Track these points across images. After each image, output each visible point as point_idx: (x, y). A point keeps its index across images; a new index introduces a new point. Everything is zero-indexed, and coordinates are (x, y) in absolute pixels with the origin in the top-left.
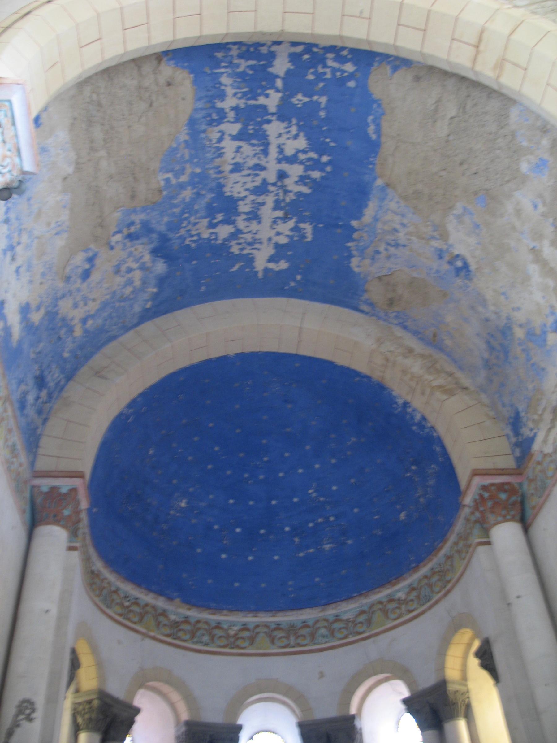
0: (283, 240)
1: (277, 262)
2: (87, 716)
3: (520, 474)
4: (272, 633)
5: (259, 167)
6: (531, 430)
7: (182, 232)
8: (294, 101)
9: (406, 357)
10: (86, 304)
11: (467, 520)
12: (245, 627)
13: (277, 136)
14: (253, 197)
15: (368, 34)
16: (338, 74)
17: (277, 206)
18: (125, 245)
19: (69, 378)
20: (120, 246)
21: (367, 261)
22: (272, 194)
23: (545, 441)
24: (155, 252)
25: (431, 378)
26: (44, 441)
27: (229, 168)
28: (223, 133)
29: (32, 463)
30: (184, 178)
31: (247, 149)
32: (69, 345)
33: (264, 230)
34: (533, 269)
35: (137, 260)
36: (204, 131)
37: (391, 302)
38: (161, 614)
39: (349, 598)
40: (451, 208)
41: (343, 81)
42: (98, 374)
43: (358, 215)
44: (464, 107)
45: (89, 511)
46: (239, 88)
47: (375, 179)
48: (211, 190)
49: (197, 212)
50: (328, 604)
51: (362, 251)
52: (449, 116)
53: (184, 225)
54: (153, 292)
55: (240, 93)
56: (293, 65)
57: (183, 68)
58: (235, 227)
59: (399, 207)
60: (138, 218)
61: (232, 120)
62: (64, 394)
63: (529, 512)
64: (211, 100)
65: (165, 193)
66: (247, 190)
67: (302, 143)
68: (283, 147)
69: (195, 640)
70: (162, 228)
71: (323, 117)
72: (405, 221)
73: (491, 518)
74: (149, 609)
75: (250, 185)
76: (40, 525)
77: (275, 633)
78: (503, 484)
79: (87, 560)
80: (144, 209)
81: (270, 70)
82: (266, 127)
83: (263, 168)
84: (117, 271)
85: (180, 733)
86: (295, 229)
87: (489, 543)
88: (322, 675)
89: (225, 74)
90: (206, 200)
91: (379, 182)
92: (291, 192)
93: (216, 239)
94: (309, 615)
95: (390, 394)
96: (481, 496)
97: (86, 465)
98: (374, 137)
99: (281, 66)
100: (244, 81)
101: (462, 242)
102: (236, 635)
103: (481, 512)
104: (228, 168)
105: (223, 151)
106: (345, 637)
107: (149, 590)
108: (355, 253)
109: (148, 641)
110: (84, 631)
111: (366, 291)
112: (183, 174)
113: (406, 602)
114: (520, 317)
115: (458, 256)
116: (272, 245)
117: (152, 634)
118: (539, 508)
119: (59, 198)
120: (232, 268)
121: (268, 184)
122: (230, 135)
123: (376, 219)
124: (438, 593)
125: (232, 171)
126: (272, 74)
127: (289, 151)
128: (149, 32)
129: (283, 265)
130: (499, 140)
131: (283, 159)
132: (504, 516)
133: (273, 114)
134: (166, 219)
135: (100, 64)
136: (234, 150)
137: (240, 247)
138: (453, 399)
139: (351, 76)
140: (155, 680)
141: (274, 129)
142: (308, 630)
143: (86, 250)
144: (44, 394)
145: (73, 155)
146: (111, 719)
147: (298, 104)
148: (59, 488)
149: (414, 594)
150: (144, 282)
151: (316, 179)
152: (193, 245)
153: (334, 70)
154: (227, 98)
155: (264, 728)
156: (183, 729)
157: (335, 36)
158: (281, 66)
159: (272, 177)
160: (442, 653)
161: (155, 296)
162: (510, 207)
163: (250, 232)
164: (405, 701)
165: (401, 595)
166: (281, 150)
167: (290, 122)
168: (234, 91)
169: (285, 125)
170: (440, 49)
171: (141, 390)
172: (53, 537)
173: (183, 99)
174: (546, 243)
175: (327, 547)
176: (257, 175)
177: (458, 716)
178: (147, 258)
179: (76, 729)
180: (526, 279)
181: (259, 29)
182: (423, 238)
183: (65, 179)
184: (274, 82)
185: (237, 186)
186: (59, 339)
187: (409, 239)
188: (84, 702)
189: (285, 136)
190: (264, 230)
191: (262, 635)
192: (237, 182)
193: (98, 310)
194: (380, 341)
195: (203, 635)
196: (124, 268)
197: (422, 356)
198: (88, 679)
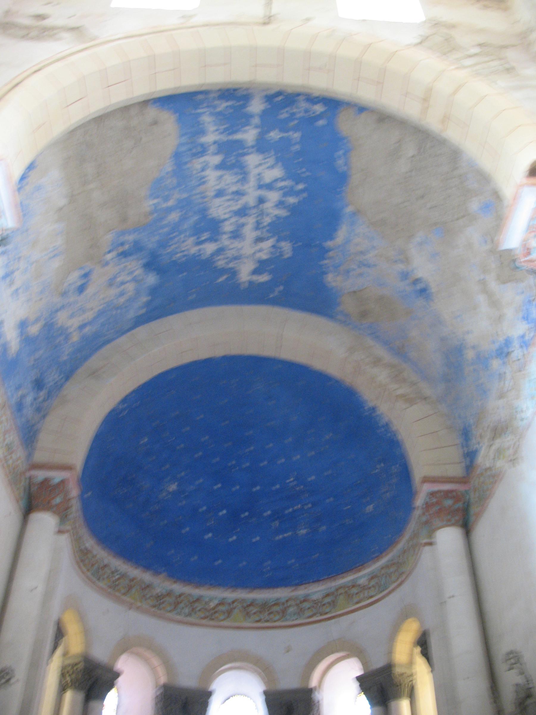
0: (264, 256)
3: (465, 483)
4: (247, 607)
5: (239, 194)
17: (258, 226)
19: (68, 377)
27: (212, 194)
29: (30, 455)
34: (481, 298)
37: (364, 314)
43: (331, 237)
45: (81, 497)
60: (131, 238)
77: (251, 608)
78: (451, 491)
79: (77, 540)
85: (158, 693)
87: (431, 544)
88: (288, 650)
91: (349, 209)
94: (281, 593)
99: (256, 107)
101: (423, 268)
102: (214, 608)
105: (206, 179)
110: (71, 603)
118: (478, 515)
129: (264, 278)
141: (252, 160)
144: (42, 394)
146: (92, 681)
150: (138, 293)
156: (161, 691)
158: (256, 107)
161: (148, 304)
165: (362, 581)
168: (215, 128)
170: (391, 101)
172: (45, 522)
175: (303, 532)
178: (139, 272)
179: (62, 689)
185: (219, 209)
198: (75, 644)
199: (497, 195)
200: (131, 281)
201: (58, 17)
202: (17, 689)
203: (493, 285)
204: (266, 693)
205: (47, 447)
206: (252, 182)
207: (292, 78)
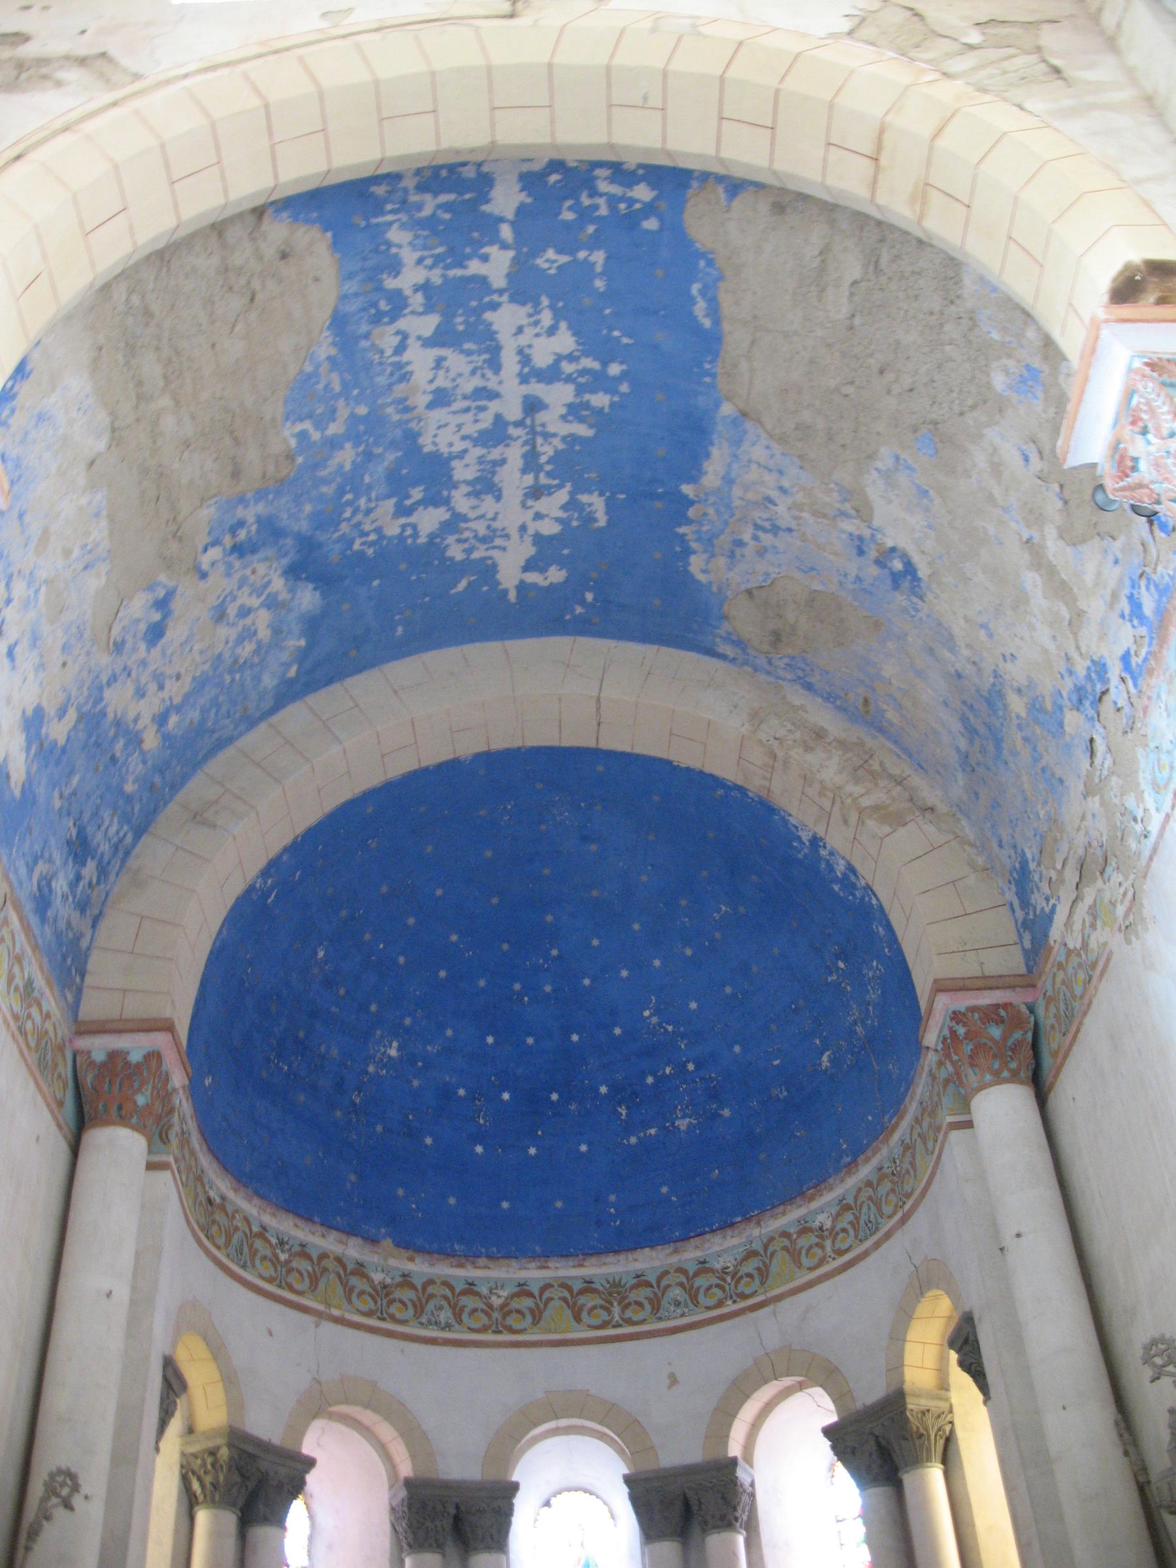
0: (549, 528)
1: (543, 570)
2: (208, 1479)
4: (575, 1299)
5: (486, 394)
6: (1047, 899)
7: (344, 527)
8: (540, 262)
9: (808, 748)
10: (161, 687)
12: (523, 1290)
13: (514, 331)
14: (479, 451)
15: (664, 140)
16: (622, 206)
17: (531, 462)
18: (230, 566)
20: (221, 568)
21: (722, 561)
22: (520, 442)
23: (1068, 924)
24: (294, 572)
25: (858, 790)
26: (95, 962)
28: (405, 336)
30: (334, 429)
31: (456, 361)
32: (136, 766)
33: (510, 511)
34: (1032, 581)
35: (257, 591)
36: (367, 336)
37: (777, 638)
40: (871, 457)
41: (631, 220)
42: (198, 818)
43: (693, 473)
44: (877, 262)
45: (194, 1088)
46: (425, 248)
47: (717, 405)
48: (393, 445)
49: (370, 487)
50: (686, 1238)
51: (709, 542)
52: (848, 280)
53: (347, 514)
54: (299, 647)
55: (432, 256)
56: (529, 195)
57: (308, 221)
58: (451, 509)
59: (772, 456)
60: (250, 514)
61: (421, 309)
62: (132, 863)
63: (1047, 1061)
64: (373, 277)
65: (300, 460)
66: (464, 438)
67: (565, 341)
68: (527, 351)
69: (424, 1320)
70: (304, 526)
71: (602, 290)
72: (786, 484)
73: (971, 1077)
74: (329, 1264)
75: (471, 429)
76: (94, 1126)
77: (582, 1300)
79: (194, 1180)
80: (261, 495)
81: (486, 208)
82: (488, 316)
83: (494, 395)
84: (220, 615)
86: (571, 505)
88: (673, 1380)
89: (396, 226)
90: (386, 464)
91: (727, 409)
92: (554, 435)
93: (415, 535)
94: (649, 1261)
95: (785, 822)
96: (953, 1033)
97: (179, 1003)
98: (707, 323)
99: (506, 199)
100: (435, 232)
101: (899, 525)
102: (503, 1306)
103: (953, 1064)
104: (422, 400)
105: (409, 368)
106: (720, 1304)
107: (328, 1225)
108: (694, 545)
109: (328, 1327)
110: (193, 1319)
111: (726, 618)
112: (334, 421)
113: (834, 1234)
114: (1015, 673)
115: (893, 550)
116: (530, 539)
117: (336, 1312)
119: (83, 501)
120: (455, 586)
121: (507, 424)
122: (419, 338)
123: (729, 481)
124: (890, 1217)
125: (430, 406)
126: (490, 215)
127: (542, 360)
128: (223, 177)
129: (556, 575)
130: (947, 328)
131: (529, 373)
132: (996, 1074)
133: (501, 292)
134: (308, 508)
135: (130, 256)
136: (433, 365)
137: (466, 546)
138: (902, 831)
139: (650, 209)
140: (347, 1402)
141: (506, 319)
142: (647, 1292)
143: (151, 588)
144: (90, 870)
145: (103, 418)
146: (253, 1484)
147: (549, 269)
148: (128, 1053)
149: (849, 1216)
150: (277, 631)
151: (603, 408)
152: (370, 552)
153: (613, 201)
154: (404, 270)
156: (403, 1493)
157: (598, 147)
158: (506, 199)
159: (513, 410)
160: (897, 1338)
161: (302, 656)
162: (980, 459)
163: (482, 517)
164: (828, 1432)
165: (824, 1219)
166: (525, 358)
167: (537, 303)
168: (416, 255)
169: (528, 308)
170: (801, 163)
171: (287, 840)
172: (118, 1149)
173: (317, 280)
174: (1051, 532)
175: (683, 1124)
176: (483, 409)
177: (929, 1460)
178: (278, 584)
179: (190, 1503)
180: (1021, 601)
181: (445, 145)
182: (825, 516)
183: (92, 463)
184: (497, 231)
185: (442, 432)
186: (113, 759)
187: (796, 518)
188: (204, 1451)
189: (529, 332)
190: (510, 511)
191: (556, 1303)
192: (446, 425)
193: (187, 696)
194: (757, 718)
195: (441, 1308)
196: (232, 611)
197: (842, 744)
198: (208, 1406)
199: (1049, 347)
200: (264, 604)
201: (50, 37)
202: (88, 1519)
203: (1053, 547)
204: (629, 1480)
205: (110, 985)
206: (510, 362)
207: (580, 131)
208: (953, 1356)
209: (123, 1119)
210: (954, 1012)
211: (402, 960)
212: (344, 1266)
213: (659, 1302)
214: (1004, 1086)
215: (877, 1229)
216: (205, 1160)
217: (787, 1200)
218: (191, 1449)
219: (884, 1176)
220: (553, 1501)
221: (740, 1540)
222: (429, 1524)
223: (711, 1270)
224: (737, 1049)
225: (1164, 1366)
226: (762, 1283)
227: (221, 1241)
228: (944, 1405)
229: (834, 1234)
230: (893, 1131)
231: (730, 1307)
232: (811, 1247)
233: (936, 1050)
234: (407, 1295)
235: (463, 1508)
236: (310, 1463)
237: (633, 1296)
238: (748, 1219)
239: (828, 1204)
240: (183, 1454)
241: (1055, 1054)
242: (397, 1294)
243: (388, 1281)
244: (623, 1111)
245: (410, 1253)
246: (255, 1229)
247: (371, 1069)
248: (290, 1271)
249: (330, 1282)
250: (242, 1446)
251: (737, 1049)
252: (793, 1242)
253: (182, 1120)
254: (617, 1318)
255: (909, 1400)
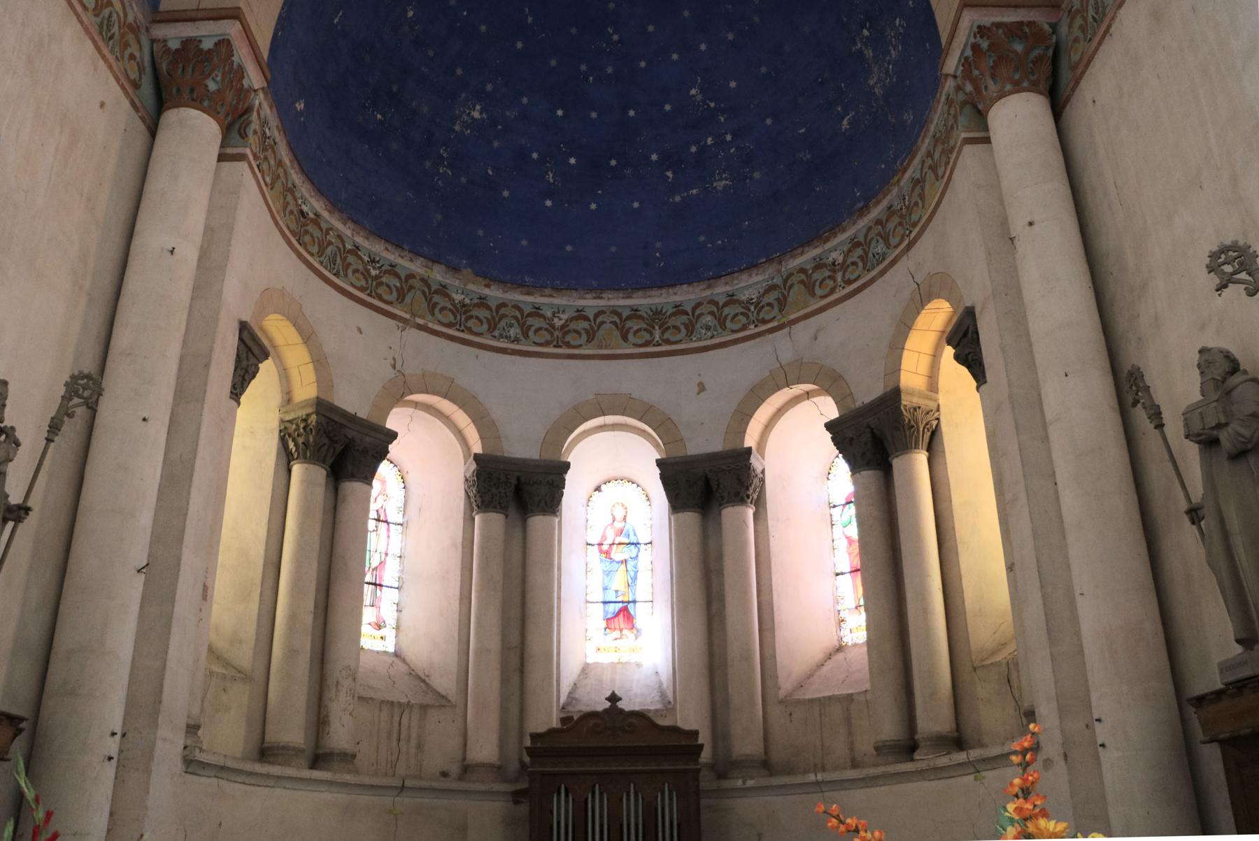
2: (301, 440)
4: (623, 324)
11: (950, 102)
12: (580, 315)
38: (436, 292)
39: (752, 266)
63: (1066, 75)
69: (496, 333)
74: (415, 282)
76: (170, 108)
77: (629, 324)
78: (1020, 24)
88: (702, 388)
94: (686, 295)
102: (563, 327)
106: (744, 328)
107: (416, 253)
109: (413, 334)
113: (844, 267)
124: (896, 247)
142: (684, 318)
149: (859, 251)
155: (618, 475)
156: (474, 466)
160: (896, 347)
164: (830, 426)
165: (837, 256)
172: (193, 131)
175: (720, 185)
191: (607, 326)
195: (511, 326)
204: (660, 463)
208: (949, 351)
209: (196, 103)
210: (979, 27)
211: (483, 28)
212: (429, 287)
213: (693, 327)
214: (1024, 94)
215: (884, 259)
216: (296, 177)
217: (807, 243)
218: (288, 418)
219: (894, 213)
220: (603, 487)
221: (750, 512)
222: (494, 490)
223: (738, 302)
224: (769, 121)
225: (1235, 273)
226: (781, 311)
227: (315, 249)
228: (932, 405)
229: (844, 267)
230: (905, 170)
231: (752, 330)
232: (824, 280)
233: (955, 77)
234: (483, 313)
235: (523, 479)
236: (393, 436)
237: (671, 322)
238: (770, 261)
239: (841, 243)
240: (282, 421)
241: (1074, 68)
242: (475, 312)
243: (467, 301)
244: (670, 174)
245: (487, 281)
246: (349, 246)
247: (457, 128)
248: (381, 284)
249: (415, 297)
250: (332, 416)
251: (769, 121)
252: (809, 277)
253: (264, 123)
254: (657, 338)
255: (903, 397)
